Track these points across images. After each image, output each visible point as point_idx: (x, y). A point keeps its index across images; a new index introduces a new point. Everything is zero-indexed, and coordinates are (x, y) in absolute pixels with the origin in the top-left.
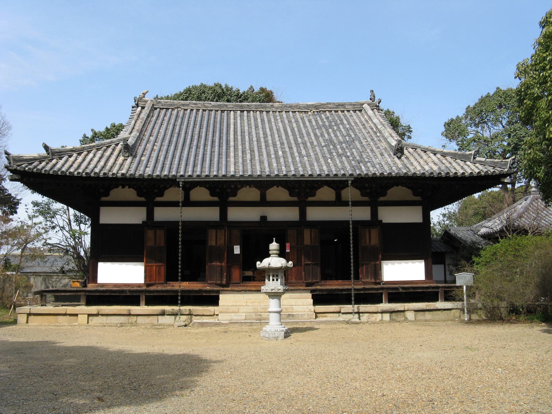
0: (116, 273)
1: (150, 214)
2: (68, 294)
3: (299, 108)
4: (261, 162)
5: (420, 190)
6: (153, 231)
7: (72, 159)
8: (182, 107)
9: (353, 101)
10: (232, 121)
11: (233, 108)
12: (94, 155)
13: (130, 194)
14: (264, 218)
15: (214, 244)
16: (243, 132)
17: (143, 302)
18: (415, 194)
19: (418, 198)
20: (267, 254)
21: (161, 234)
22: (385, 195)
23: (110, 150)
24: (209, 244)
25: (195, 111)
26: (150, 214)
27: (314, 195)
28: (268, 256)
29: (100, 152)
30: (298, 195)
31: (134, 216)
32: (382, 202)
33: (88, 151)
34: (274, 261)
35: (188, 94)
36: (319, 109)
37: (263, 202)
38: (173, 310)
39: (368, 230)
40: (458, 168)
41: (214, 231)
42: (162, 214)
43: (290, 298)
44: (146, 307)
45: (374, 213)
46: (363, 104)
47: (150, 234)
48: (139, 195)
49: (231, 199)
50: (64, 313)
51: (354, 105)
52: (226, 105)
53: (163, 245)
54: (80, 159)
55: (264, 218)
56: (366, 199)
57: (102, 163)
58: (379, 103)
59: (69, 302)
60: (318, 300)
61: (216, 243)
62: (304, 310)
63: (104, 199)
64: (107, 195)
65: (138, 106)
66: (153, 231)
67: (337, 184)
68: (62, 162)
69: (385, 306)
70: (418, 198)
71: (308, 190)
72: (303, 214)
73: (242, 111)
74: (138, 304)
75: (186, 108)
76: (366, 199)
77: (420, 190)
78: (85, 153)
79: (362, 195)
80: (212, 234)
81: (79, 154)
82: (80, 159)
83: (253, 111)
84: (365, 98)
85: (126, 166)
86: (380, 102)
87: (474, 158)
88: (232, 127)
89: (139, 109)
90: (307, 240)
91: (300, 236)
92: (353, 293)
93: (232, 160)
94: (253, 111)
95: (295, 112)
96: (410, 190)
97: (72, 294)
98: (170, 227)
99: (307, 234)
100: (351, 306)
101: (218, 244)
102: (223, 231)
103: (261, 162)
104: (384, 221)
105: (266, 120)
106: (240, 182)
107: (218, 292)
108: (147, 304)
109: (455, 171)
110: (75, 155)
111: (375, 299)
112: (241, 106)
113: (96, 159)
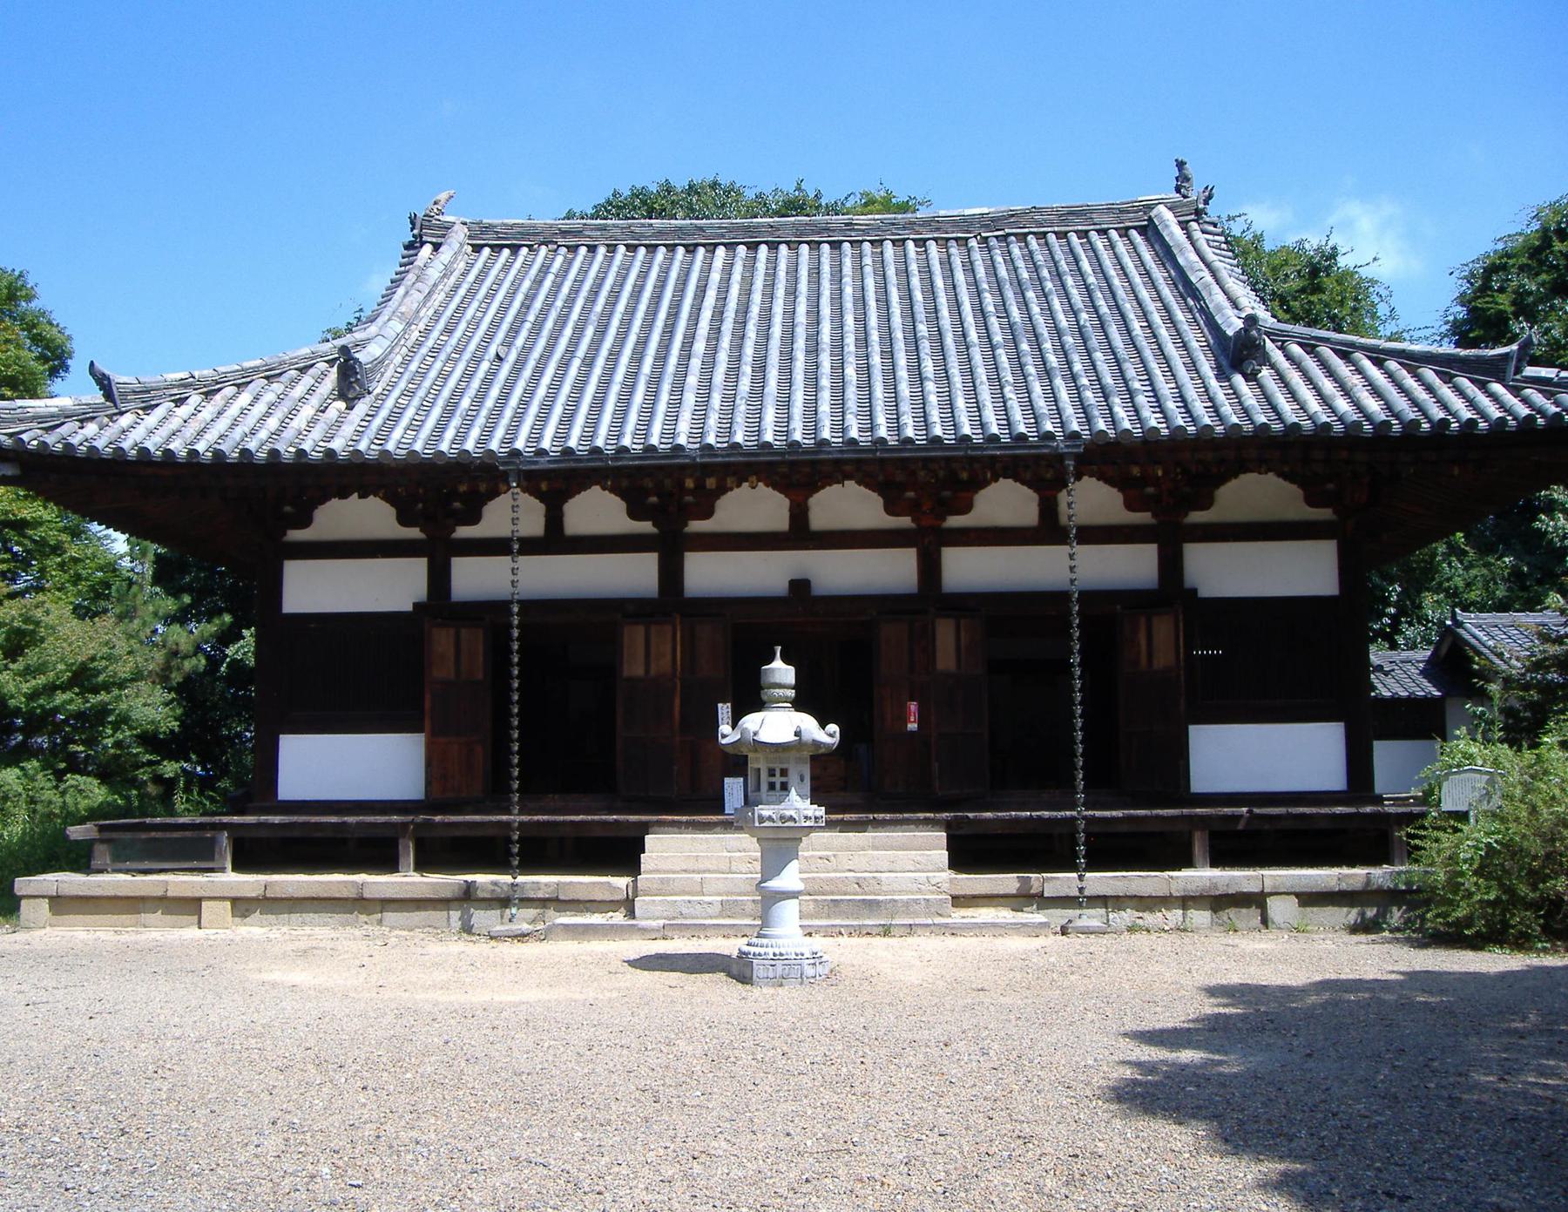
0: (325, 766)
1: (439, 578)
2: (176, 835)
3: (938, 229)
4: (785, 404)
5: (1330, 486)
6: (452, 631)
7: (184, 411)
8: (561, 241)
9: (1119, 197)
10: (715, 277)
11: (723, 236)
12: (256, 399)
13: (369, 516)
14: (800, 586)
15: (639, 671)
16: (743, 309)
17: (408, 855)
18: (1311, 501)
19: (1324, 514)
20: (751, 699)
21: (475, 639)
22: (1206, 503)
23: (307, 380)
24: (626, 673)
25: (602, 250)
26: (439, 578)
27: (966, 508)
28: (758, 705)
29: (277, 387)
30: (912, 509)
31: (393, 587)
32: (1196, 526)
33: (238, 386)
34: (779, 724)
35: (615, 207)
36: (1000, 229)
37: (800, 535)
38: (495, 883)
39: (1143, 620)
40: (1458, 404)
41: (639, 631)
42: (475, 578)
43: (875, 848)
44: (416, 878)
45: (1171, 565)
46: (1150, 207)
47: (442, 640)
48: (404, 520)
49: (696, 526)
50: (160, 894)
51: (1121, 211)
52: (701, 229)
53: (480, 676)
54: (208, 412)
55: (800, 586)
56: (1143, 517)
57: (273, 423)
58: (1206, 202)
59: (198, 859)
60: (964, 856)
61: (647, 671)
62: (915, 887)
63: (295, 535)
64: (305, 521)
65: (423, 243)
66: (452, 631)
67: (1040, 465)
68: (151, 420)
69: (1202, 876)
70: (1324, 514)
71: (947, 494)
72: (930, 568)
73: (753, 247)
74: (389, 864)
75: (572, 241)
76: (1143, 517)
77: (1330, 486)
78: (229, 391)
79: (1130, 506)
80: (634, 637)
81: (209, 395)
82: (208, 412)
83: (787, 243)
84: (1158, 190)
85: (348, 430)
86: (1210, 197)
87: (1518, 370)
88: (711, 294)
89: (427, 249)
90: (946, 659)
91: (924, 641)
92: (1082, 825)
93: (690, 398)
94: (787, 243)
95: (925, 240)
96: (1294, 488)
97: (188, 834)
98: (489, 613)
99: (945, 634)
100: (1075, 875)
101: (653, 672)
102: (668, 628)
103: (785, 404)
104: (1205, 592)
105: (826, 268)
106: (705, 470)
107: (645, 828)
108: (422, 865)
109: (1441, 415)
110: (195, 399)
111: (1165, 851)
112: (747, 230)
113: (260, 408)
